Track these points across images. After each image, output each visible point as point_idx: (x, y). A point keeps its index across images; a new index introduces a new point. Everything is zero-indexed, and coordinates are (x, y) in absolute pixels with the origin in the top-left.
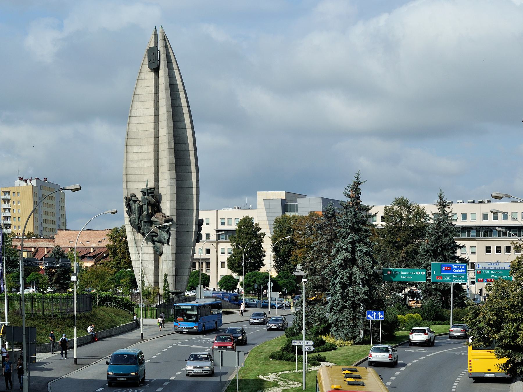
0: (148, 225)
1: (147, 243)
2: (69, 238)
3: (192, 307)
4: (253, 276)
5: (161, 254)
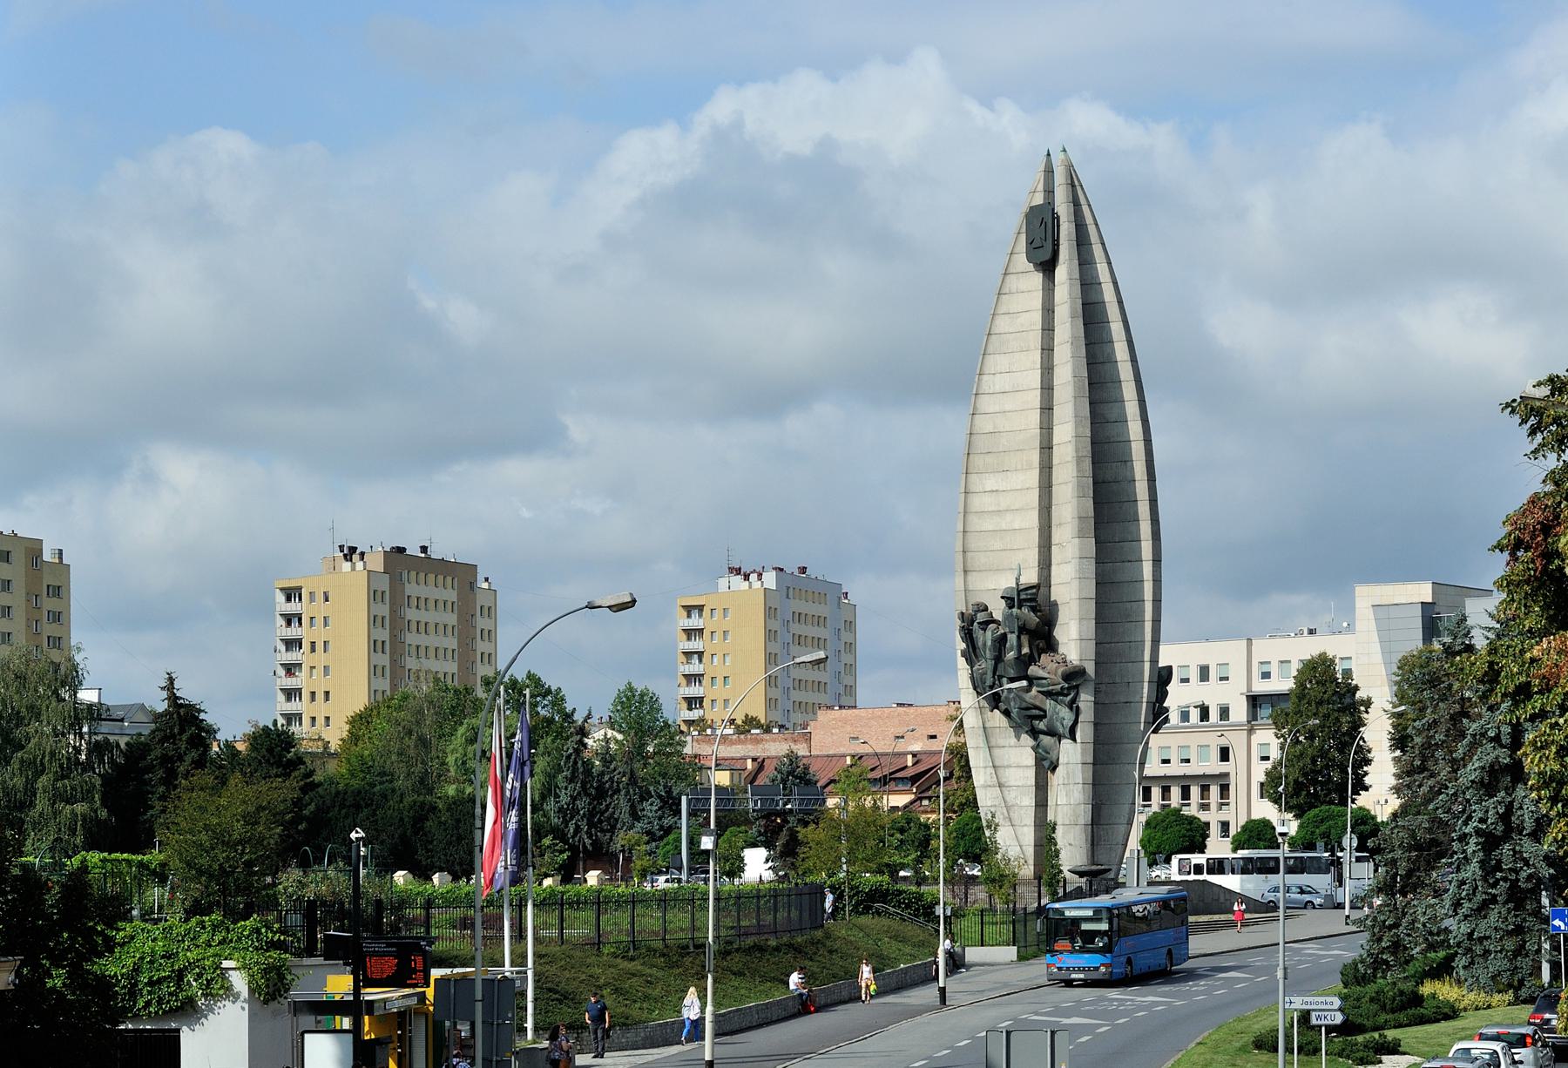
1: (1018, 737)
2: (849, 728)
3: (1097, 911)
4: (1322, 821)
5: (1054, 767)
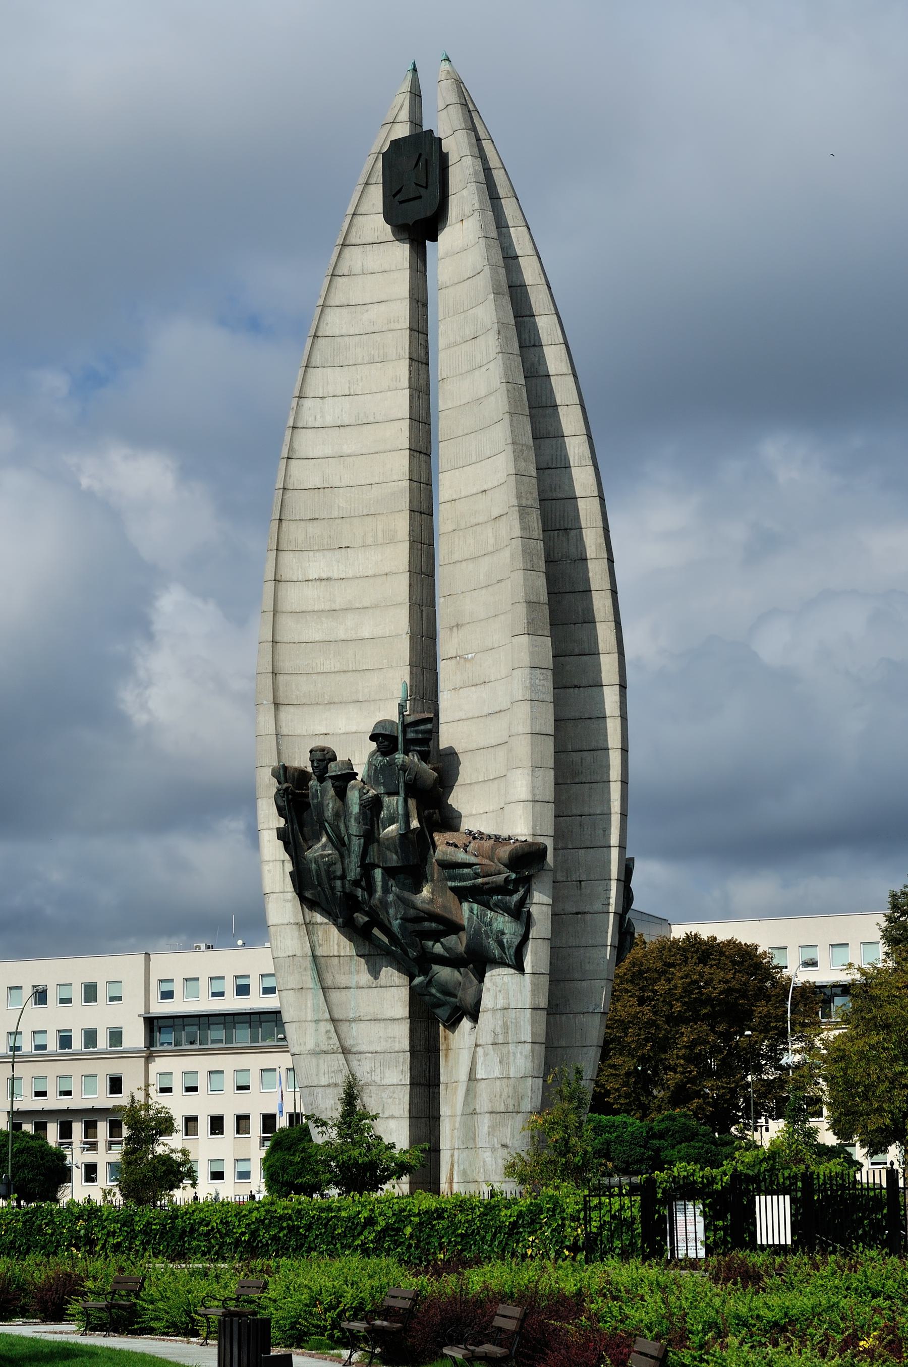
0: (403, 887)
